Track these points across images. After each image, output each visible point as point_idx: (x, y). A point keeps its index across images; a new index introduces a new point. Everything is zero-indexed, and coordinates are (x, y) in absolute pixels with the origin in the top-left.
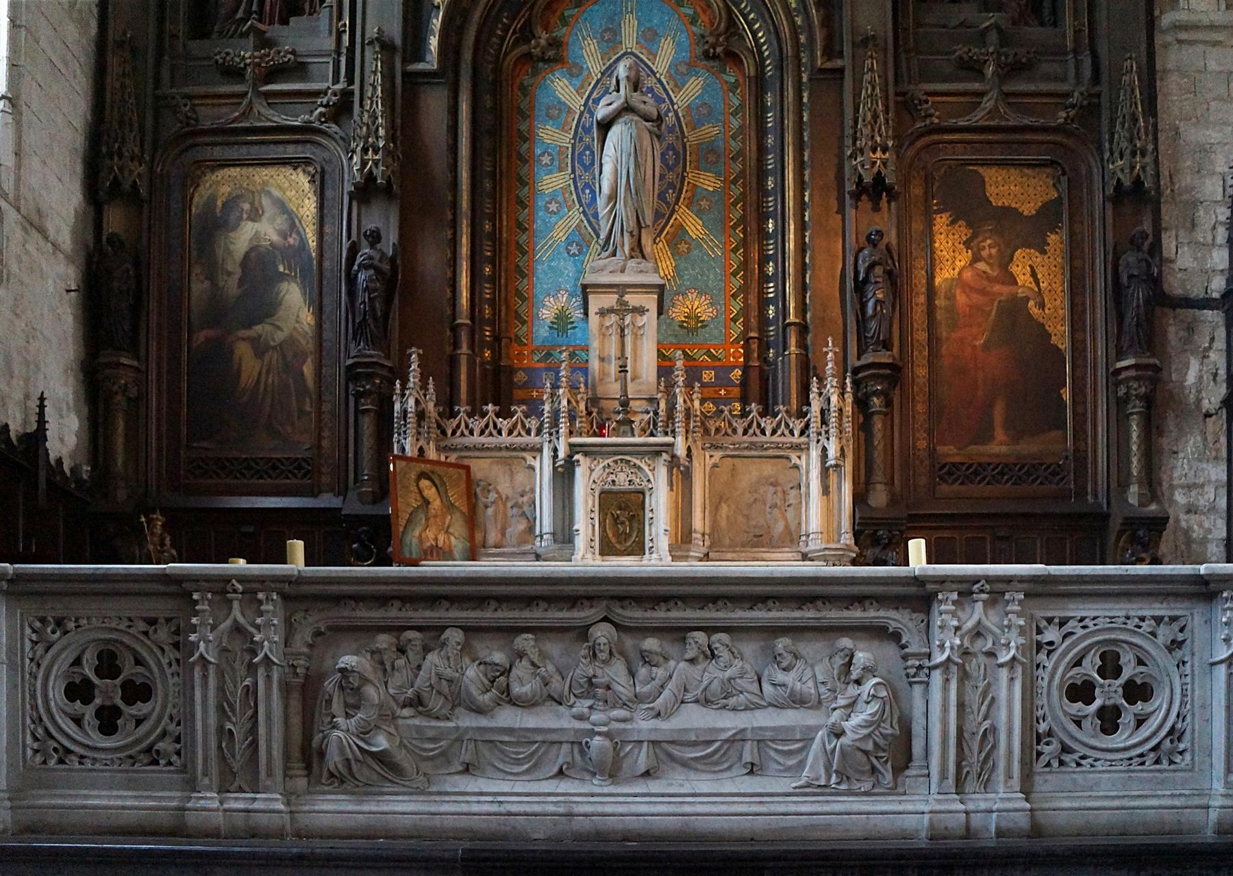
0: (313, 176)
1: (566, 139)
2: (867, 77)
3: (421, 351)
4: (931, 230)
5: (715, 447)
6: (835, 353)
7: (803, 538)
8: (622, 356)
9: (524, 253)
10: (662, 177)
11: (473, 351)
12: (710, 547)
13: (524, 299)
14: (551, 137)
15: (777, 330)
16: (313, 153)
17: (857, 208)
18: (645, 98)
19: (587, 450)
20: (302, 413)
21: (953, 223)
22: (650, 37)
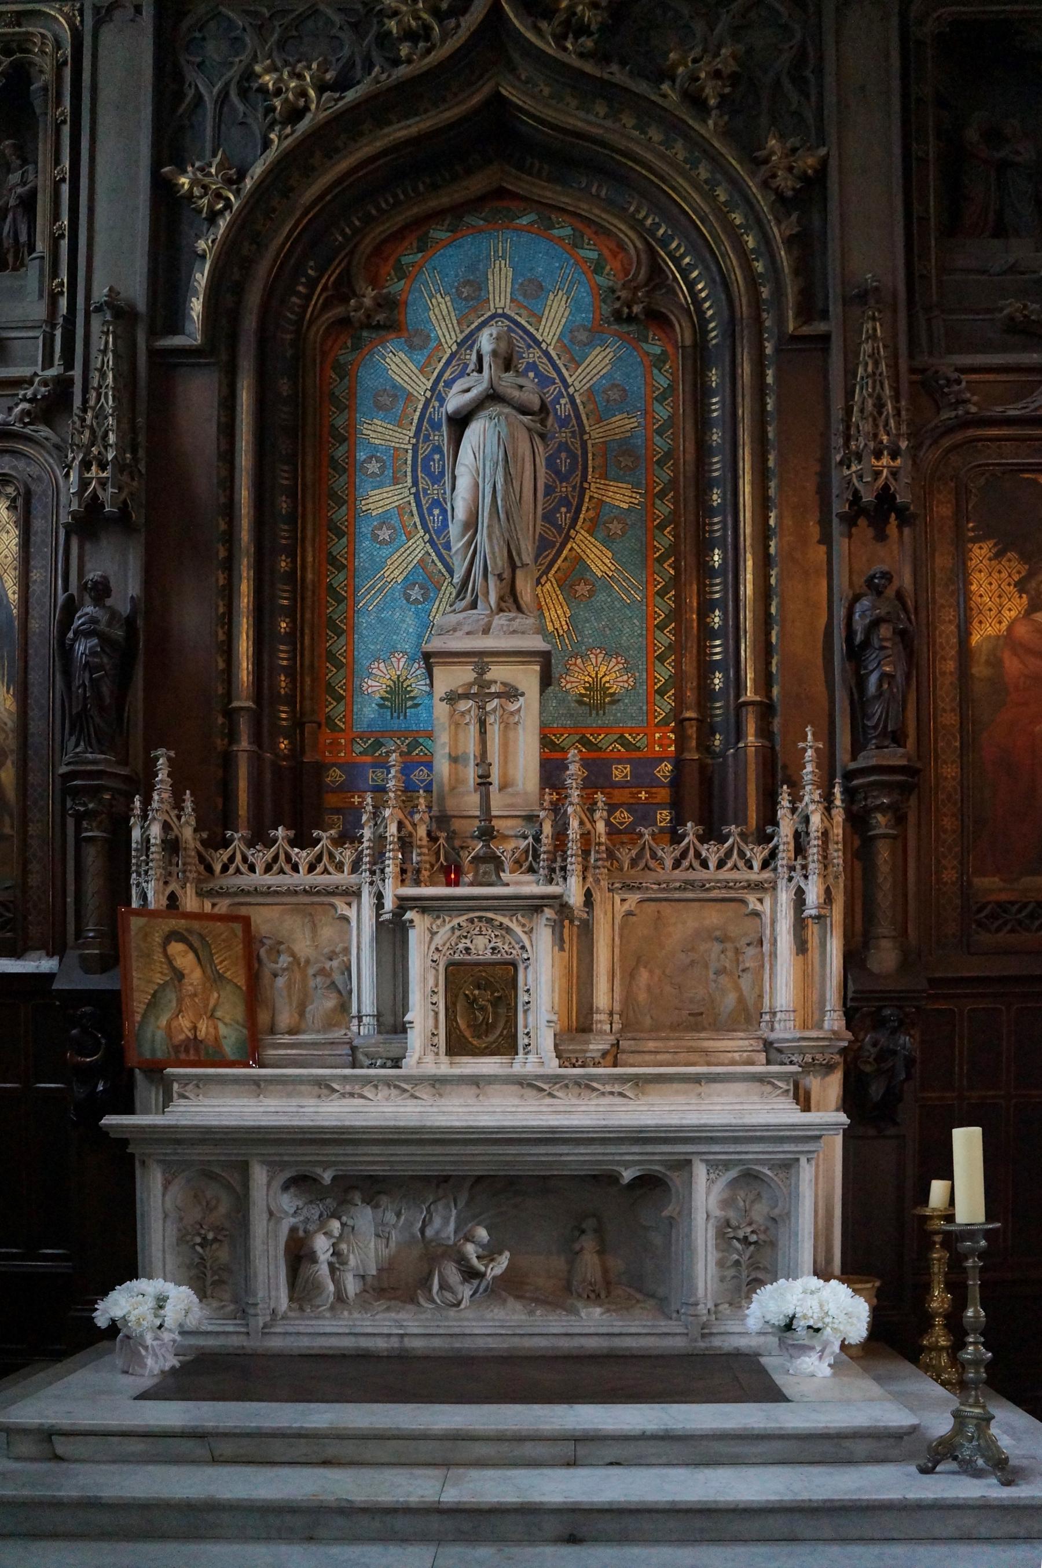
0: (14, 500)
1: (404, 438)
2: (867, 347)
3: (172, 754)
4: (964, 564)
5: (627, 887)
6: (817, 750)
7: (767, 1018)
8: (483, 759)
9: (340, 600)
10: (549, 490)
11: (260, 747)
12: (622, 1031)
13: (339, 666)
14: (380, 434)
15: (726, 707)
16: (14, 468)
17: (850, 536)
18: (521, 381)
19: (425, 906)
21: (998, 555)
22: (532, 291)
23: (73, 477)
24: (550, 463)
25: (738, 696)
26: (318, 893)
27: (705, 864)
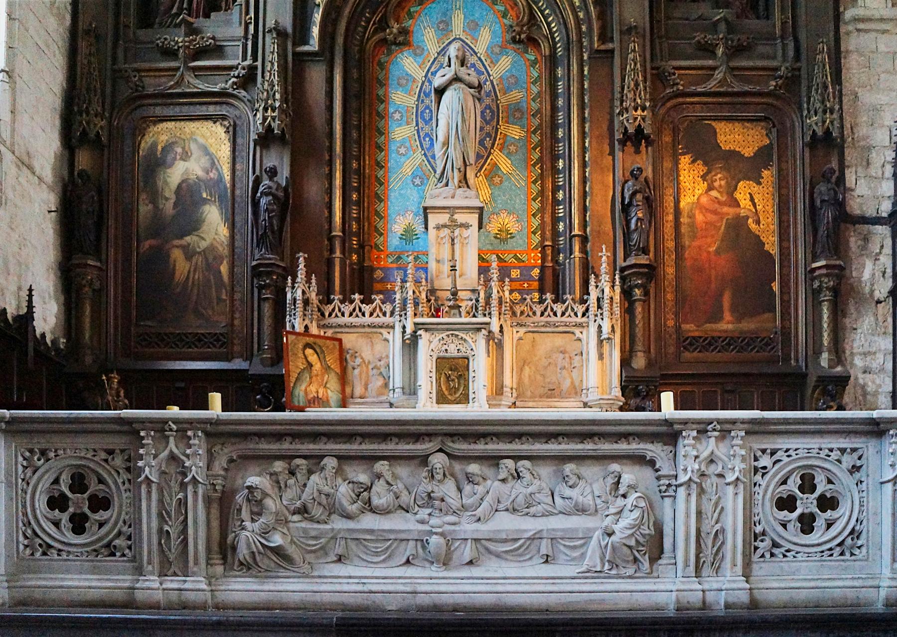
0: (228, 128)
2: (631, 56)
3: (306, 256)
4: (677, 168)
5: (520, 325)
7: (584, 391)
8: (453, 259)
10: (482, 129)
11: (344, 255)
12: (517, 398)
13: (381, 218)
14: (401, 100)
16: (228, 111)
17: (623, 151)
18: (469, 72)
20: (219, 300)
21: (693, 162)
22: (473, 27)
23: (259, 115)
24: (483, 116)
25: (571, 232)
26: (374, 327)
27: (555, 314)
